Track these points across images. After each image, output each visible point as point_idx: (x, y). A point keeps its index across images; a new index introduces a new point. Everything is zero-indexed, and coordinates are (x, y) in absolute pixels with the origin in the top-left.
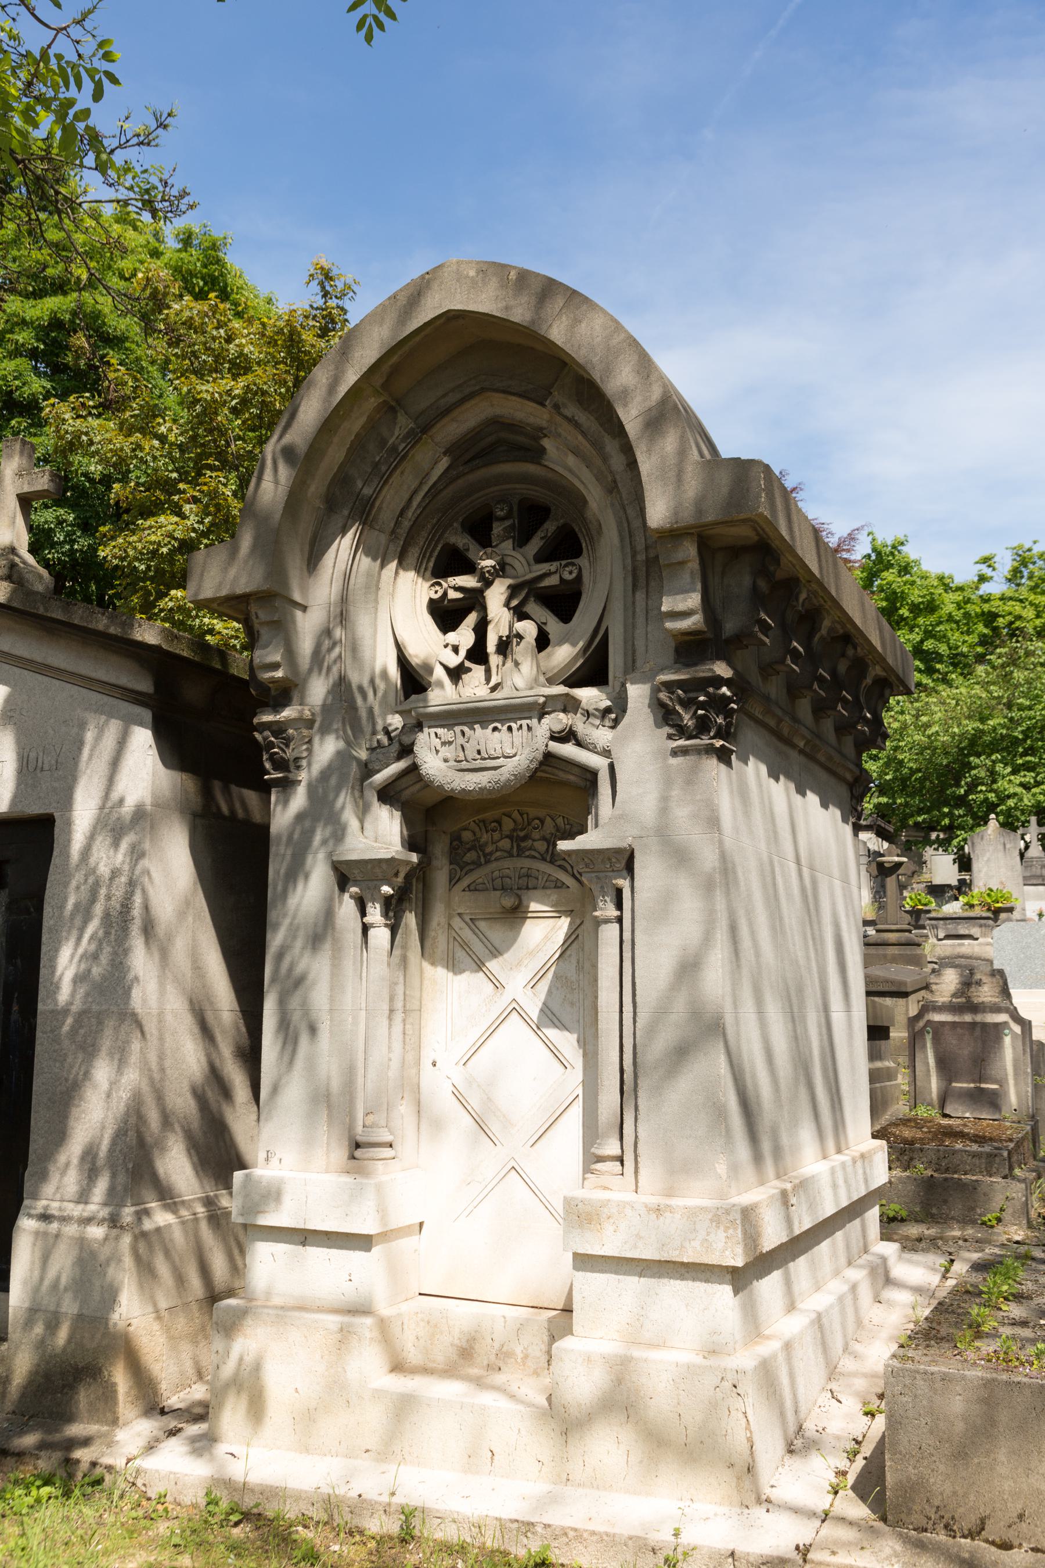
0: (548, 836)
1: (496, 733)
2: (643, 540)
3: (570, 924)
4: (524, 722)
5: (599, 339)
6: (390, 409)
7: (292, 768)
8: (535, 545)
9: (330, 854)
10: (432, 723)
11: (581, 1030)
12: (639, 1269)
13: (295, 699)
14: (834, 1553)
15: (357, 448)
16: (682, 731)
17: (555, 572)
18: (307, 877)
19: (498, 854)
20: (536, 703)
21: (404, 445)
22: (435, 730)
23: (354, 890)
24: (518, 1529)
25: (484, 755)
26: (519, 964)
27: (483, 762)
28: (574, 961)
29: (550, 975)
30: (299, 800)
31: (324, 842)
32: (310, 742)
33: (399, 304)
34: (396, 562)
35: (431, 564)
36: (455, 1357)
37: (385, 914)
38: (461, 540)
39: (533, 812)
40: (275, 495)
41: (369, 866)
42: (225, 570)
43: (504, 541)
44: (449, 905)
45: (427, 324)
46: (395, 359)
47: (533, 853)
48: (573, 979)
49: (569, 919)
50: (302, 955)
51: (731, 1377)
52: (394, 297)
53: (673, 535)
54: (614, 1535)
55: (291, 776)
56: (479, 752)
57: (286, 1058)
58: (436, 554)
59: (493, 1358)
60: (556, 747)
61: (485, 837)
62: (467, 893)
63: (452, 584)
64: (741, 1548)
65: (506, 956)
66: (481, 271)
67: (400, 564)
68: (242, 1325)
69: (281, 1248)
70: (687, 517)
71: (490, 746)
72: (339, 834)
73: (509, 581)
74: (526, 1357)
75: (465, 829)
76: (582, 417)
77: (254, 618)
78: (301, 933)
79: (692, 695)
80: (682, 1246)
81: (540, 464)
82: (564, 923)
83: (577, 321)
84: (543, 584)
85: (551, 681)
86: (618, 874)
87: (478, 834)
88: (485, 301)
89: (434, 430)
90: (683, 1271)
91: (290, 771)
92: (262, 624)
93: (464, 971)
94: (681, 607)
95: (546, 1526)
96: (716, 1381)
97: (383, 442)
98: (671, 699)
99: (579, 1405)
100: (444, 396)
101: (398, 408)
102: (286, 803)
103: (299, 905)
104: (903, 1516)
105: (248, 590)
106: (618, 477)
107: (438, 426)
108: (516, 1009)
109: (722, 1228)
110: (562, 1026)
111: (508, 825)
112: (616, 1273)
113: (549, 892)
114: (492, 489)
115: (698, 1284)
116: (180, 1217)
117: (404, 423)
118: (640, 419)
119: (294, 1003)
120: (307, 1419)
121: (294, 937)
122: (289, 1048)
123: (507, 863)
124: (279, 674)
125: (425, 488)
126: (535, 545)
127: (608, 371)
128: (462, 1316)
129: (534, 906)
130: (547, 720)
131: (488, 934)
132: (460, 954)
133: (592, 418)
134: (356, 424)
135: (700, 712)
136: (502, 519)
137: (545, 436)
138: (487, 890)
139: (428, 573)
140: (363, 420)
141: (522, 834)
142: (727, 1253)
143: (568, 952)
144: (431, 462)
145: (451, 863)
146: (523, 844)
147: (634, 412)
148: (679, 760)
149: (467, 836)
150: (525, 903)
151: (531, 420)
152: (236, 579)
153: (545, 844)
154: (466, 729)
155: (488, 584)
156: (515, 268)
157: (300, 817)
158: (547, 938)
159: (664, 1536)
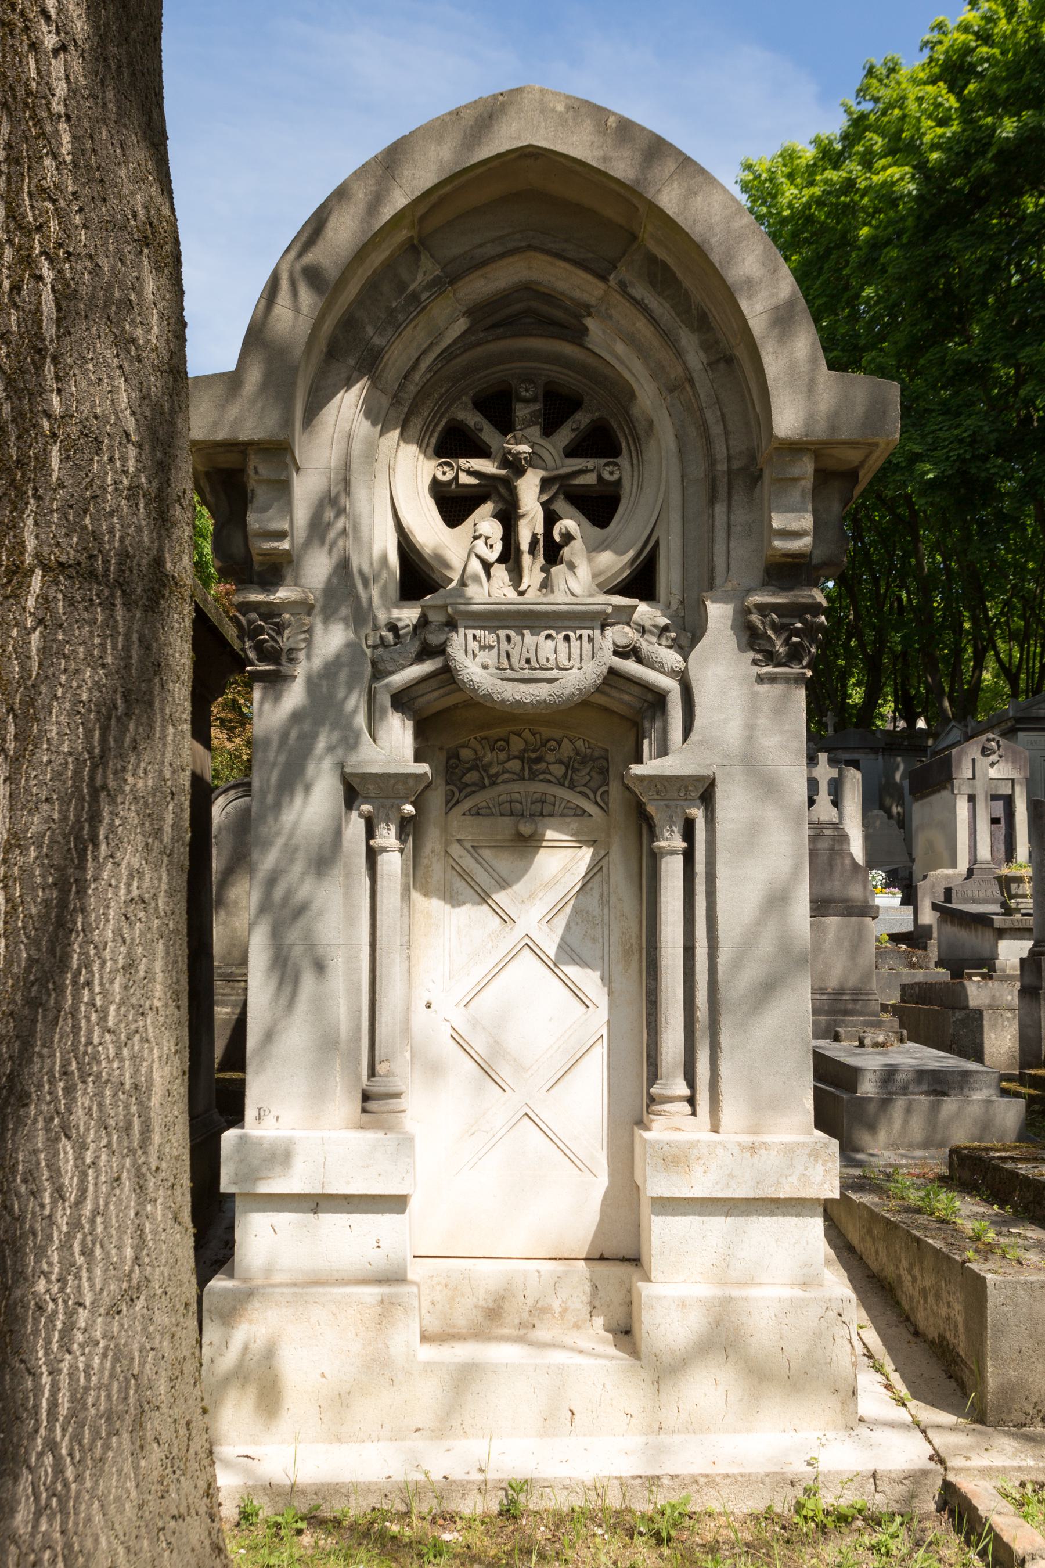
0: (565, 760)
1: (549, 642)
2: (724, 449)
3: (593, 855)
4: (585, 633)
5: (717, 218)
6: (414, 249)
7: (284, 660)
8: (565, 436)
9: (341, 765)
10: (471, 623)
11: (606, 967)
12: (725, 1209)
13: (289, 579)
14: (968, 1458)
15: (372, 286)
16: (770, 657)
17: (592, 471)
18: (308, 789)
19: (506, 776)
20: (604, 612)
21: (428, 294)
22: (474, 631)
23: (366, 808)
24: (642, 1485)
25: (534, 663)
26: (532, 896)
27: (534, 671)
28: (596, 894)
29: (568, 909)
30: (294, 696)
31: (331, 749)
32: (310, 631)
33: (463, 122)
34: (398, 431)
35: (434, 441)
36: (480, 1319)
37: (401, 836)
38: (472, 418)
39: (546, 732)
40: (294, 326)
41: (392, 781)
42: (222, 407)
43: (529, 426)
44: (451, 832)
45: (499, 156)
46: (448, 189)
47: (548, 777)
48: (596, 913)
49: (591, 850)
50: (302, 881)
51: (836, 1307)
52: (457, 113)
53: (793, 448)
54: (750, 1475)
55: (285, 669)
56: (528, 661)
57: (283, 1001)
58: (439, 428)
59: (525, 1315)
60: (619, 663)
61: (489, 757)
62: (469, 818)
63: (466, 466)
64: (881, 1467)
65: (515, 887)
66: (568, 108)
67: (402, 434)
68: (246, 1309)
69: (284, 1219)
70: (820, 432)
71: (542, 655)
72: (350, 741)
73: (542, 473)
74: (565, 1310)
75: (463, 746)
76: (653, 302)
77: (251, 472)
78: (301, 856)
79: (785, 620)
80: (778, 1183)
81: (582, 346)
82: (586, 855)
83: (692, 193)
84: (576, 482)
85: (610, 592)
86: (690, 801)
87: (481, 753)
88: (579, 145)
89: (460, 284)
90: (773, 1207)
91: (280, 664)
92: (259, 482)
93: (464, 903)
94: (795, 526)
95: (673, 1477)
96: (821, 1311)
97: (402, 287)
98: (763, 622)
99: (673, 1352)
100: (481, 246)
101: (421, 248)
102: (277, 698)
103: (296, 823)
104: (1003, 1416)
105: (256, 438)
106: (695, 375)
107: (467, 279)
108: (530, 946)
109: (820, 1162)
110: (582, 962)
111: (517, 745)
112: (700, 1214)
113: (568, 820)
114: (514, 365)
115: (788, 1219)
116: (859, 1164)
117: (427, 270)
118: (765, 316)
119: (293, 935)
120: (339, 1404)
121: (292, 861)
122: (288, 989)
123: (517, 786)
124: (285, 545)
125: (438, 350)
126: (565, 436)
127: (729, 255)
128: (488, 1275)
129: (550, 834)
130: (609, 632)
131: (494, 863)
132: (459, 884)
133: (667, 305)
134: (378, 258)
135: (795, 639)
136: (527, 401)
137: (590, 314)
138: (492, 814)
139: (430, 450)
140: (387, 253)
141: (533, 755)
142: (826, 1186)
143: (590, 885)
144: (447, 321)
145: (448, 784)
146: (535, 767)
147: (759, 308)
148: (765, 688)
149: (466, 754)
150: (540, 831)
151: (577, 294)
152: (238, 421)
153: (563, 769)
154: (512, 633)
155: (520, 472)
156: (614, 114)
157: (296, 717)
158: (566, 870)
159: (798, 1467)
